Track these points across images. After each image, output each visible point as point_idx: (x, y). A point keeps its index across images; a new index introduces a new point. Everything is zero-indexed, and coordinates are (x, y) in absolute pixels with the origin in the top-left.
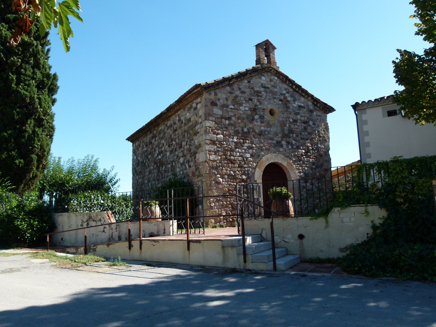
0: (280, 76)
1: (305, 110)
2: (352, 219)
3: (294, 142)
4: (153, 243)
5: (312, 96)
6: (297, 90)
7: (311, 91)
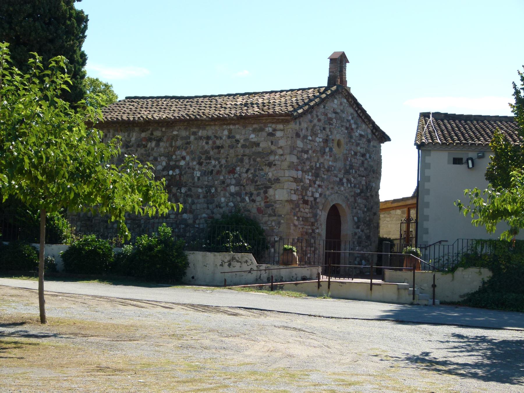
0: (349, 98)
1: (365, 140)
2: (470, 276)
3: (352, 179)
4: (340, 284)
5: (373, 123)
6: (361, 115)
7: (373, 118)
